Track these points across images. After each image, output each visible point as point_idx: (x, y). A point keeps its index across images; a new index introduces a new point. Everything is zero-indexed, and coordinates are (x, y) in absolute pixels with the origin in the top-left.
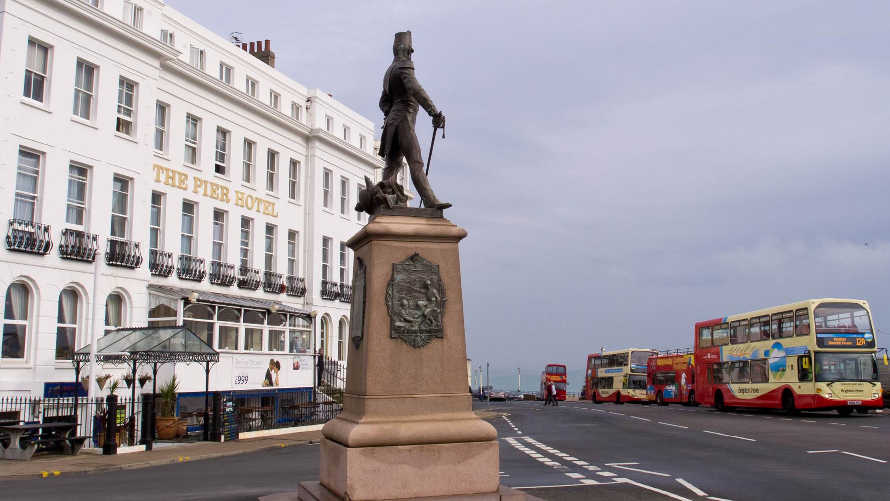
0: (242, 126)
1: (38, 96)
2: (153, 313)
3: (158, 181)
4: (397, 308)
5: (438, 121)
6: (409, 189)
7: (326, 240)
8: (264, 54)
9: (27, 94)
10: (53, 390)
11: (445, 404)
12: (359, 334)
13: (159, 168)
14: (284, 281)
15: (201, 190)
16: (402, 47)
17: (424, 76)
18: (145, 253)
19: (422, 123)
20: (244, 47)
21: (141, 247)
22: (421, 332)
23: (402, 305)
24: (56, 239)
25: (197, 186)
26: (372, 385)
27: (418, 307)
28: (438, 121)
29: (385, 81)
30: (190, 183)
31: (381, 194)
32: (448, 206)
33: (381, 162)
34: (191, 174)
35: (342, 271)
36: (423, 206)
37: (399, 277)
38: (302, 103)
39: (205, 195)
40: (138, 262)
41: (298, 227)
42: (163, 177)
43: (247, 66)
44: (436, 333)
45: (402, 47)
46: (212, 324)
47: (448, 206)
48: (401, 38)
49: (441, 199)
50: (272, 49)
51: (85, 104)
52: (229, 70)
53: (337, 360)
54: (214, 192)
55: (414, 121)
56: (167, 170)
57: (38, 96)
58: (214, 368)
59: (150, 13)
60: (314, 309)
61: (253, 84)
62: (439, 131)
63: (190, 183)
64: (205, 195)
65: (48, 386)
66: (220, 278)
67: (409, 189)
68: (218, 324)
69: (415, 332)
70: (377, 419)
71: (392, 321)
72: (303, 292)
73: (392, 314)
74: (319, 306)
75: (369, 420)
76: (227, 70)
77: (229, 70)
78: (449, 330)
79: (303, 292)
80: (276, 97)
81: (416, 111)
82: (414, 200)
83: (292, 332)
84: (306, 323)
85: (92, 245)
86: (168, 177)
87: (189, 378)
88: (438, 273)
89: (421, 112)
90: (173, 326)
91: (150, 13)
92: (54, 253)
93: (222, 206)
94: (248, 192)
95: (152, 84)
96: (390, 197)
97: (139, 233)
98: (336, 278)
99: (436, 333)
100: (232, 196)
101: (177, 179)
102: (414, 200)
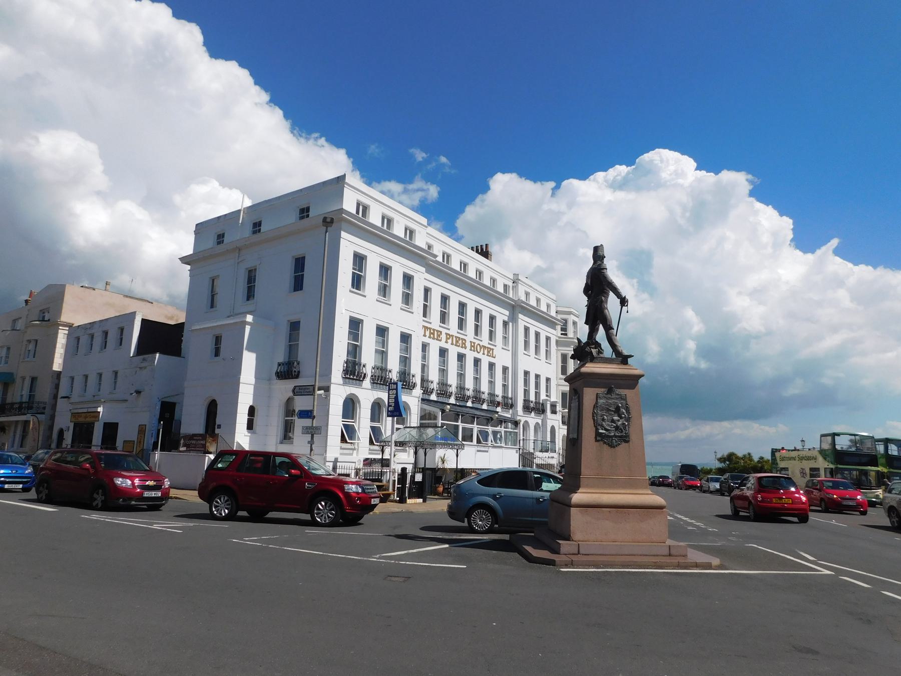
0: (473, 302)
1: (358, 288)
2: (422, 418)
3: (425, 336)
4: (600, 421)
5: (623, 302)
6: (605, 345)
7: (526, 373)
8: (484, 252)
9: (353, 286)
10: (368, 462)
11: (631, 485)
12: (575, 436)
13: (426, 328)
14: (499, 399)
15: (450, 341)
16: (598, 255)
17: (614, 274)
18: (418, 380)
19: (612, 302)
20: (472, 249)
21: (367, 366)
22: (616, 436)
23: (603, 420)
24: (368, 371)
25: (447, 339)
26: (585, 471)
27: (613, 421)
28: (623, 302)
29: (588, 276)
30: (443, 336)
31: (587, 349)
32: (631, 356)
33: (586, 328)
34: (444, 331)
35: (504, 386)
36: (614, 356)
37: (601, 401)
38: (510, 284)
39: (452, 344)
40: (414, 386)
41: (509, 364)
42: (428, 333)
43: (476, 262)
44: (625, 439)
45: (598, 255)
46: (458, 426)
47: (631, 356)
48: (596, 249)
49: (626, 353)
50: (490, 250)
51: (384, 290)
52: (448, 256)
53: (532, 451)
54: (459, 342)
55: (607, 302)
56: (430, 329)
57: (358, 288)
58: (461, 453)
59: (420, 232)
60: (518, 418)
61: (480, 273)
62: (624, 308)
63: (443, 336)
64: (452, 344)
65: (366, 460)
66: (493, 402)
67: (605, 345)
68: (461, 425)
69: (611, 437)
70: (628, 491)
71: (597, 429)
72: (512, 406)
73: (596, 425)
74: (521, 416)
75: (584, 491)
76: (464, 266)
77: (448, 256)
78: (633, 437)
79: (512, 406)
80: (538, 300)
81: (608, 295)
82: (608, 351)
83: (505, 432)
84: (513, 426)
85: (450, 390)
86: (430, 333)
87: (447, 458)
88: (625, 400)
89: (611, 294)
90: (435, 426)
91: (398, 222)
92: (367, 383)
93: (462, 351)
94: (477, 342)
95: (422, 277)
96: (594, 351)
97: (368, 359)
98: (532, 398)
99: (625, 439)
100: (468, 345)
101: (435, 334)
102: (608, 351)
